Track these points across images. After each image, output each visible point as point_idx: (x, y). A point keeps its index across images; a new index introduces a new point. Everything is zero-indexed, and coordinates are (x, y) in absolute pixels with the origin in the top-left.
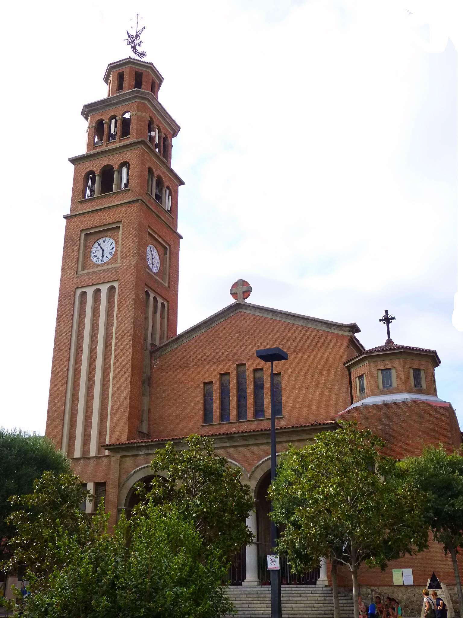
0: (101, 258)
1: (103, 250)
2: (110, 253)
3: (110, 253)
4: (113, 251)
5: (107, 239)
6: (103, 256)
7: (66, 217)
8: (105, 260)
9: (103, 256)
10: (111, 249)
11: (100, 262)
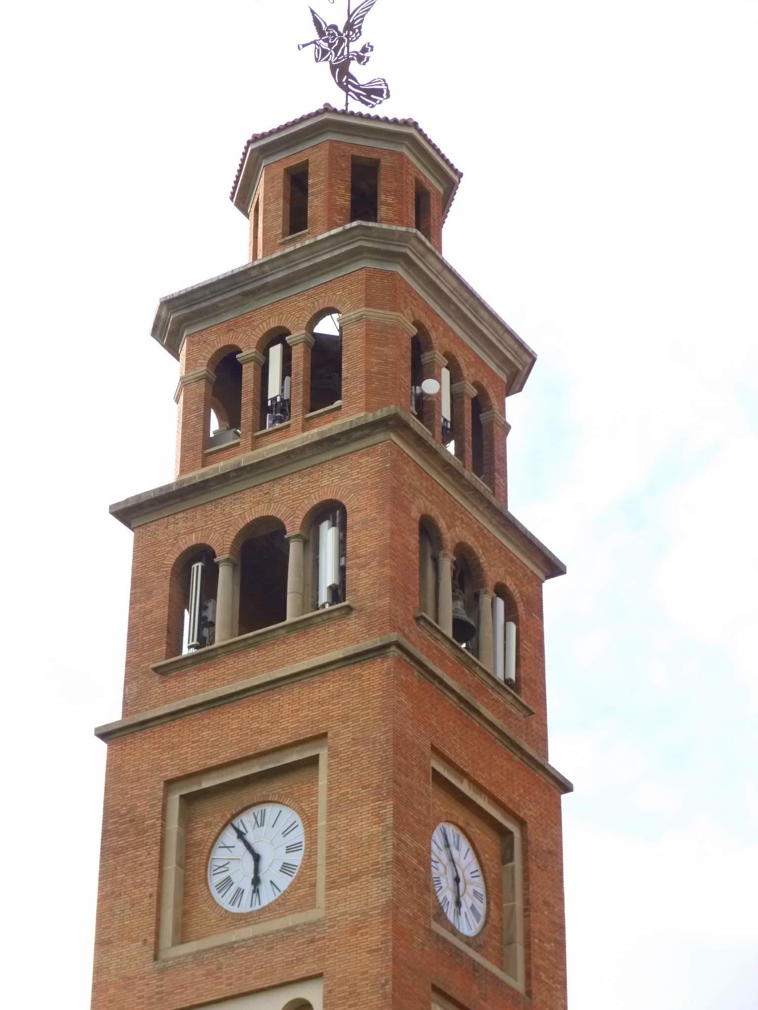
0: (248, 888)
1: (257, 858)
2: (286, 868)
3: (286, 868)
4: (297, 858)
5: (271, 811)
6: (256, 881)
7: (106, 734)
8: (268, 896)
9: (256, 881)
10: (290, 849)
11: (245, 906)
